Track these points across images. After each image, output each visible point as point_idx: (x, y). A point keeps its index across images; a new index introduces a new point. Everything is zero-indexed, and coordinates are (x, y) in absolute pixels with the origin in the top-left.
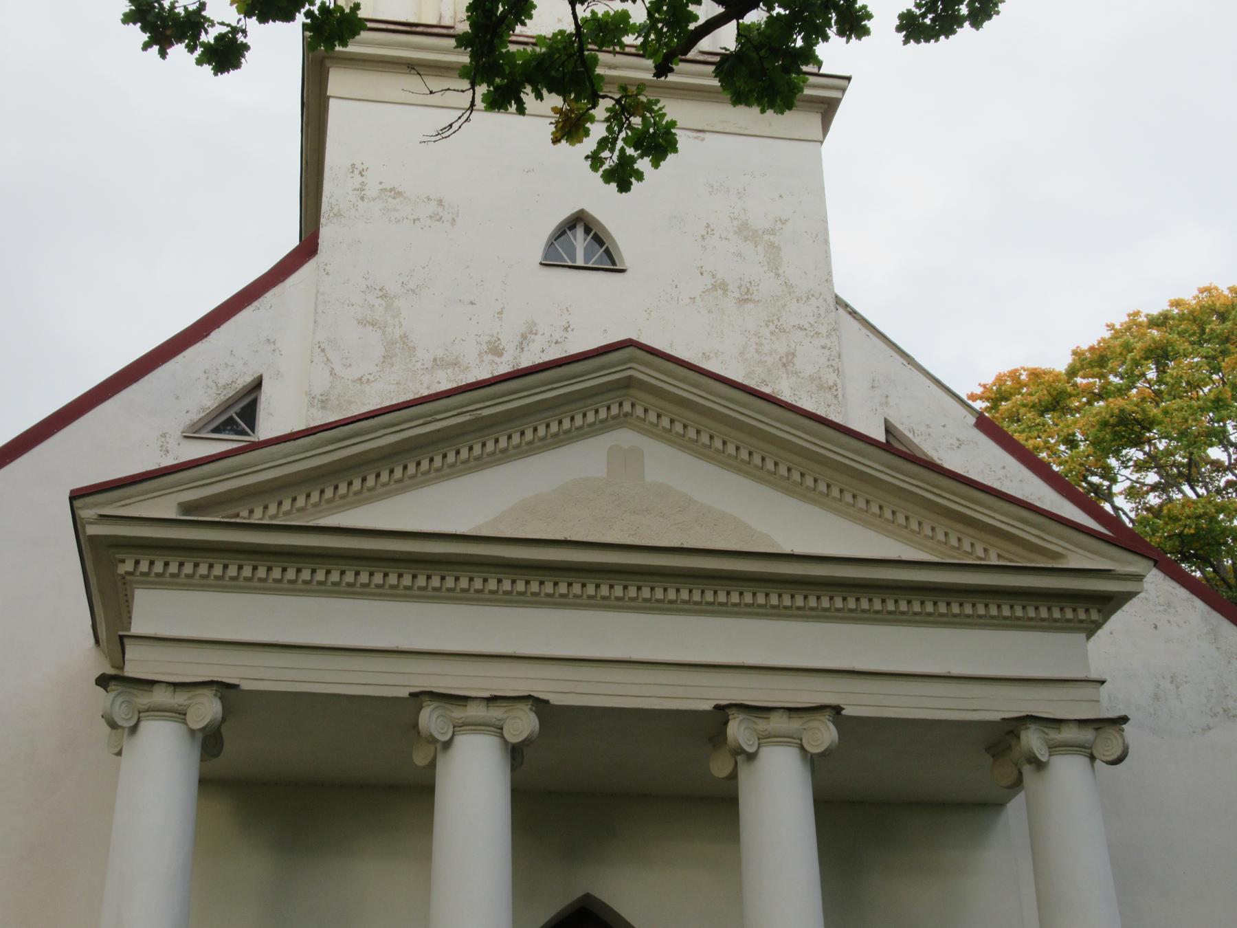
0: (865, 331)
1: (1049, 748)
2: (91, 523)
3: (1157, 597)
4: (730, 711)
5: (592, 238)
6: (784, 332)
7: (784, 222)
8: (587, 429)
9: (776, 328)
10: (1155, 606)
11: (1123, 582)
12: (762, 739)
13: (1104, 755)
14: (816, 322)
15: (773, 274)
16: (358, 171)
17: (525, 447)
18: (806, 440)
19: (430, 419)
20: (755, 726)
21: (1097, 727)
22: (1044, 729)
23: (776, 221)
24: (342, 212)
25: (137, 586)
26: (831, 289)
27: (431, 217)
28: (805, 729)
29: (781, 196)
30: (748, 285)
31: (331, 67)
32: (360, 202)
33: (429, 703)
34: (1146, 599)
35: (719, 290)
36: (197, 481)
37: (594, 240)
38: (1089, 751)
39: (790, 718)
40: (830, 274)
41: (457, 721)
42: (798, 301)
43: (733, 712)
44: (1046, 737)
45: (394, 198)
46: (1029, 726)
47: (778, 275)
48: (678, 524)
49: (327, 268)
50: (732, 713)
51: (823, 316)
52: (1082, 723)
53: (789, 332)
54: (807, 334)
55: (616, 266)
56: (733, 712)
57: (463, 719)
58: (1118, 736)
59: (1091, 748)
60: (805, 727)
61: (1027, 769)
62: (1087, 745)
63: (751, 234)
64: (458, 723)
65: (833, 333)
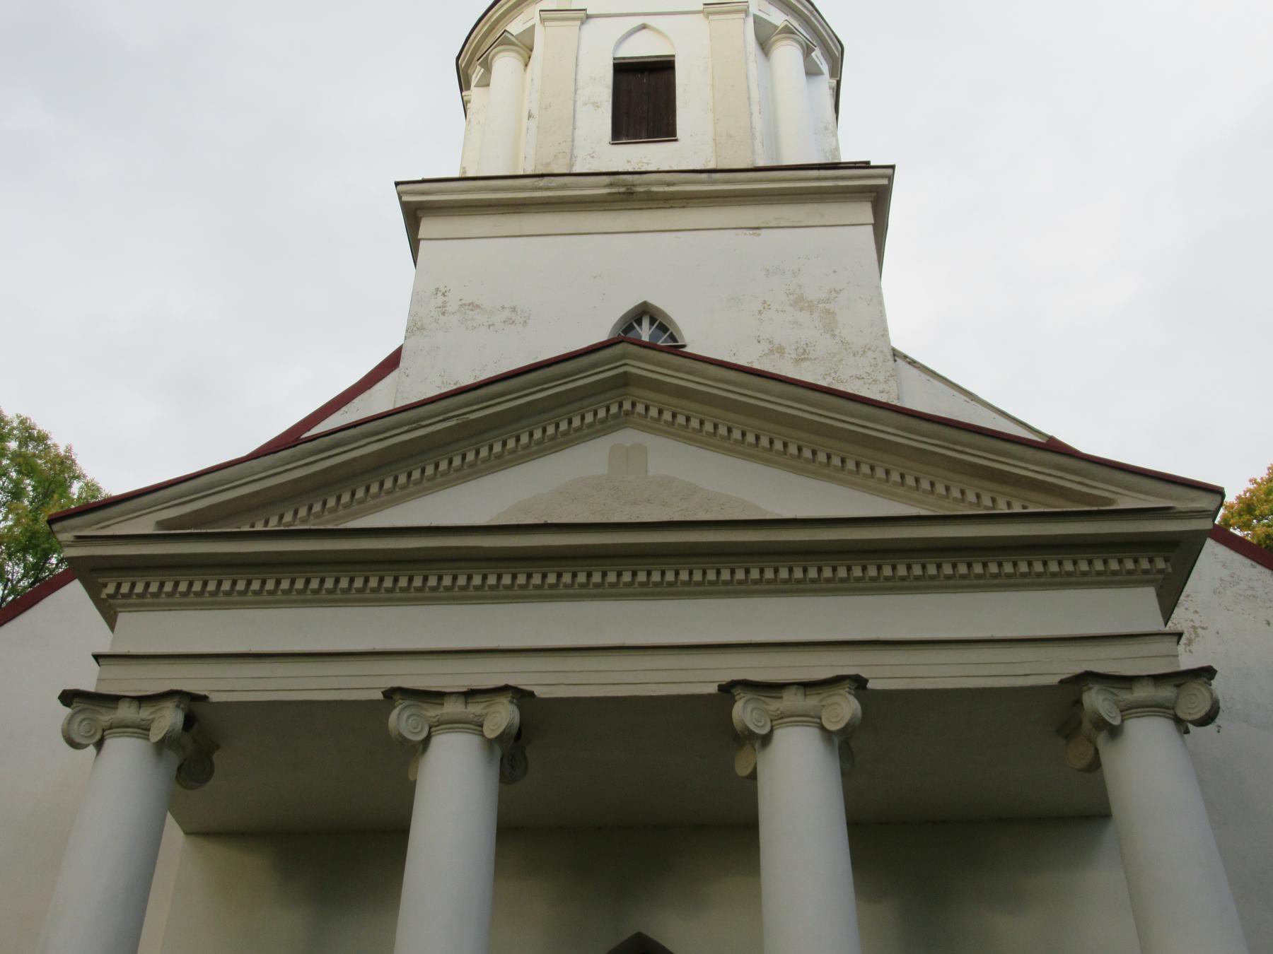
0: (925, 377)
1: (1121, 711)
2: (68, 546)
3: (1266, 593)
4: (736, 691)
5: (657, 327)
6: (842, 382)
7: (838, 292)
8: (586, 431)
9: (834, 380)
10: (1265, 602)
11: (1187, 521)
12: (776, 720)
13: (1190, 714)
14: (873, 371)
15: (829, 336)
16: (441, 293)
17: (521, 452)
18: (812, 413)
19: (414, 425)
20: (767, 707)
21: (1176, 682)
22: (1112, 690)
23: (831, 292)
24: (424, 326)
25: (119, 610)
26: (888, 342)
27: (504, 321)
28: (823, 706)
29: (835, 272)
30: (805, 346)
31: (423, 217)
32: (441, 316)
33: (400, 701)
34: (1254, 596)
35: (776, 354)
36: (175, 500)
37: (659, 329)
38: (1172, 712)
39: (806, 695)
40: (886, 329)
41: (432, 719)
42: (854, 355)
43: (738, 692)
44: (1116, 698)
45: (472, 310)
46: (1090, 685)
47: (834, 336)
48: (682, 510)
49: (407, 372)
50: (737, 691)
51: (880, 365)
52: (1158, 679)
53: (846, 382)
54: (865, 382)
55: (677, 342)
56: (738, 692)
57: (438, 717)
58: (1203, 689)
59: (1173, 708)
60: (823, 703)
61: (1101, 739)
62: (1167, 704)
63: (806, 305)
64: (434, 722)
65: (891, 379)
